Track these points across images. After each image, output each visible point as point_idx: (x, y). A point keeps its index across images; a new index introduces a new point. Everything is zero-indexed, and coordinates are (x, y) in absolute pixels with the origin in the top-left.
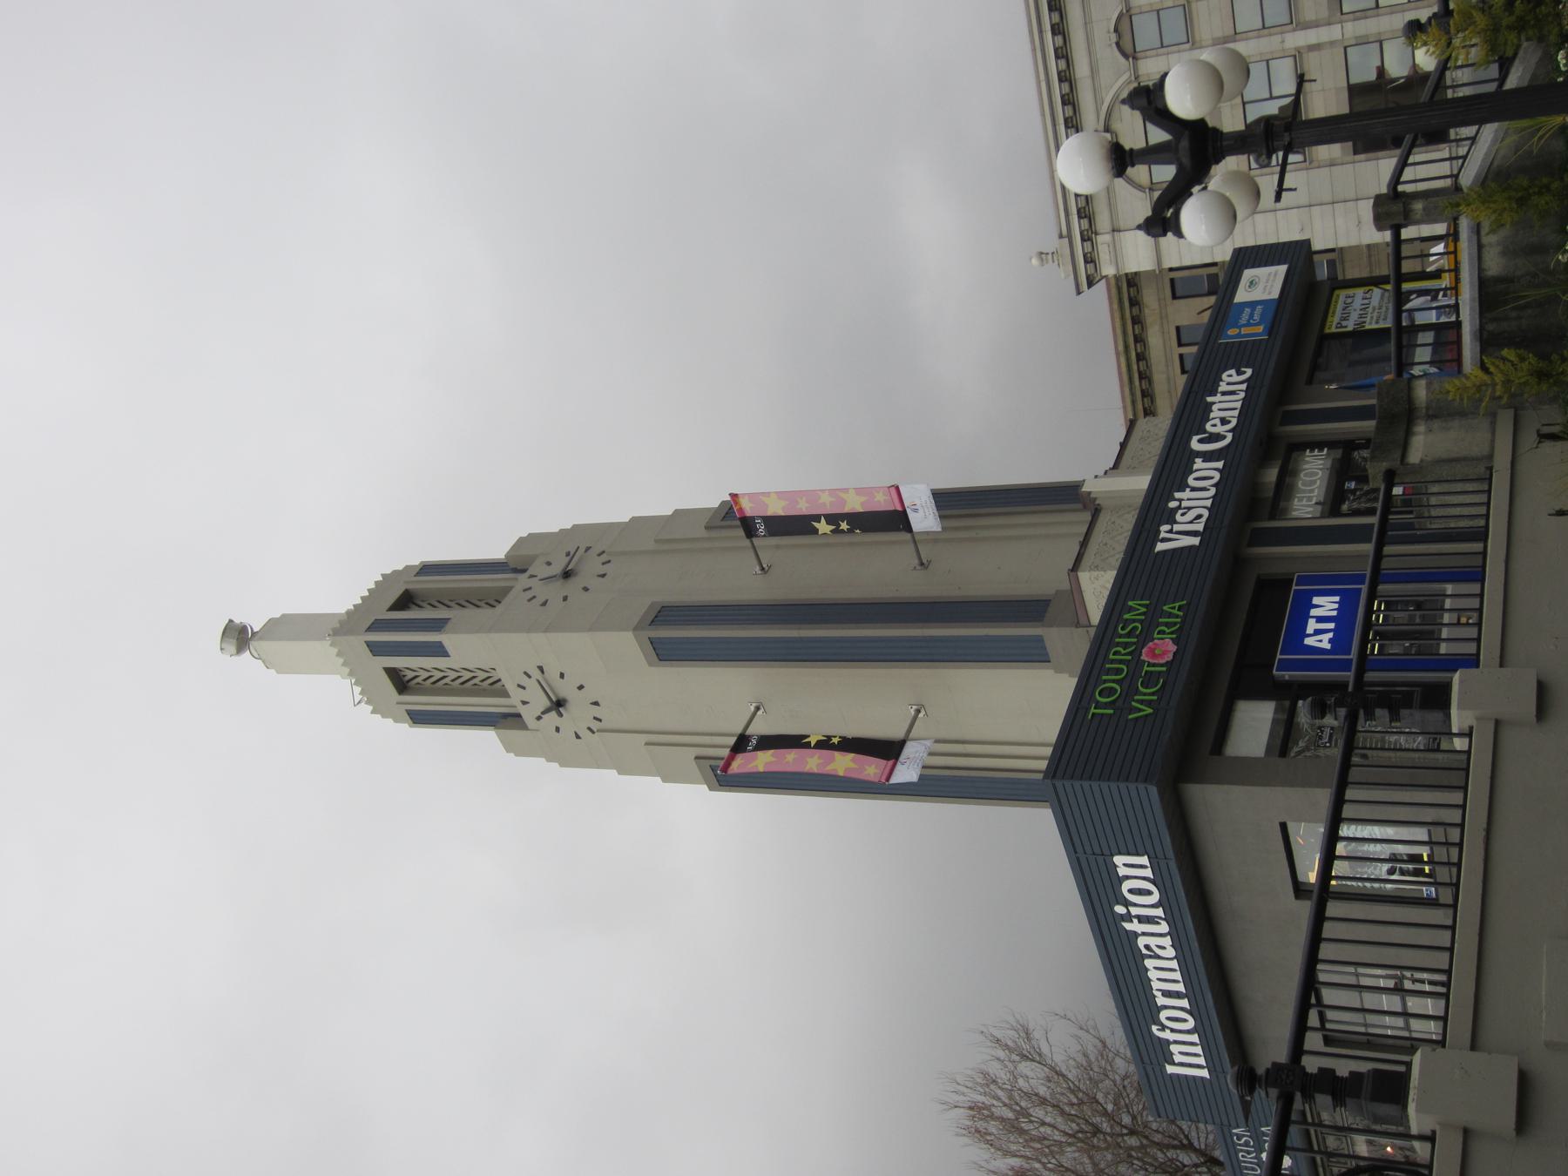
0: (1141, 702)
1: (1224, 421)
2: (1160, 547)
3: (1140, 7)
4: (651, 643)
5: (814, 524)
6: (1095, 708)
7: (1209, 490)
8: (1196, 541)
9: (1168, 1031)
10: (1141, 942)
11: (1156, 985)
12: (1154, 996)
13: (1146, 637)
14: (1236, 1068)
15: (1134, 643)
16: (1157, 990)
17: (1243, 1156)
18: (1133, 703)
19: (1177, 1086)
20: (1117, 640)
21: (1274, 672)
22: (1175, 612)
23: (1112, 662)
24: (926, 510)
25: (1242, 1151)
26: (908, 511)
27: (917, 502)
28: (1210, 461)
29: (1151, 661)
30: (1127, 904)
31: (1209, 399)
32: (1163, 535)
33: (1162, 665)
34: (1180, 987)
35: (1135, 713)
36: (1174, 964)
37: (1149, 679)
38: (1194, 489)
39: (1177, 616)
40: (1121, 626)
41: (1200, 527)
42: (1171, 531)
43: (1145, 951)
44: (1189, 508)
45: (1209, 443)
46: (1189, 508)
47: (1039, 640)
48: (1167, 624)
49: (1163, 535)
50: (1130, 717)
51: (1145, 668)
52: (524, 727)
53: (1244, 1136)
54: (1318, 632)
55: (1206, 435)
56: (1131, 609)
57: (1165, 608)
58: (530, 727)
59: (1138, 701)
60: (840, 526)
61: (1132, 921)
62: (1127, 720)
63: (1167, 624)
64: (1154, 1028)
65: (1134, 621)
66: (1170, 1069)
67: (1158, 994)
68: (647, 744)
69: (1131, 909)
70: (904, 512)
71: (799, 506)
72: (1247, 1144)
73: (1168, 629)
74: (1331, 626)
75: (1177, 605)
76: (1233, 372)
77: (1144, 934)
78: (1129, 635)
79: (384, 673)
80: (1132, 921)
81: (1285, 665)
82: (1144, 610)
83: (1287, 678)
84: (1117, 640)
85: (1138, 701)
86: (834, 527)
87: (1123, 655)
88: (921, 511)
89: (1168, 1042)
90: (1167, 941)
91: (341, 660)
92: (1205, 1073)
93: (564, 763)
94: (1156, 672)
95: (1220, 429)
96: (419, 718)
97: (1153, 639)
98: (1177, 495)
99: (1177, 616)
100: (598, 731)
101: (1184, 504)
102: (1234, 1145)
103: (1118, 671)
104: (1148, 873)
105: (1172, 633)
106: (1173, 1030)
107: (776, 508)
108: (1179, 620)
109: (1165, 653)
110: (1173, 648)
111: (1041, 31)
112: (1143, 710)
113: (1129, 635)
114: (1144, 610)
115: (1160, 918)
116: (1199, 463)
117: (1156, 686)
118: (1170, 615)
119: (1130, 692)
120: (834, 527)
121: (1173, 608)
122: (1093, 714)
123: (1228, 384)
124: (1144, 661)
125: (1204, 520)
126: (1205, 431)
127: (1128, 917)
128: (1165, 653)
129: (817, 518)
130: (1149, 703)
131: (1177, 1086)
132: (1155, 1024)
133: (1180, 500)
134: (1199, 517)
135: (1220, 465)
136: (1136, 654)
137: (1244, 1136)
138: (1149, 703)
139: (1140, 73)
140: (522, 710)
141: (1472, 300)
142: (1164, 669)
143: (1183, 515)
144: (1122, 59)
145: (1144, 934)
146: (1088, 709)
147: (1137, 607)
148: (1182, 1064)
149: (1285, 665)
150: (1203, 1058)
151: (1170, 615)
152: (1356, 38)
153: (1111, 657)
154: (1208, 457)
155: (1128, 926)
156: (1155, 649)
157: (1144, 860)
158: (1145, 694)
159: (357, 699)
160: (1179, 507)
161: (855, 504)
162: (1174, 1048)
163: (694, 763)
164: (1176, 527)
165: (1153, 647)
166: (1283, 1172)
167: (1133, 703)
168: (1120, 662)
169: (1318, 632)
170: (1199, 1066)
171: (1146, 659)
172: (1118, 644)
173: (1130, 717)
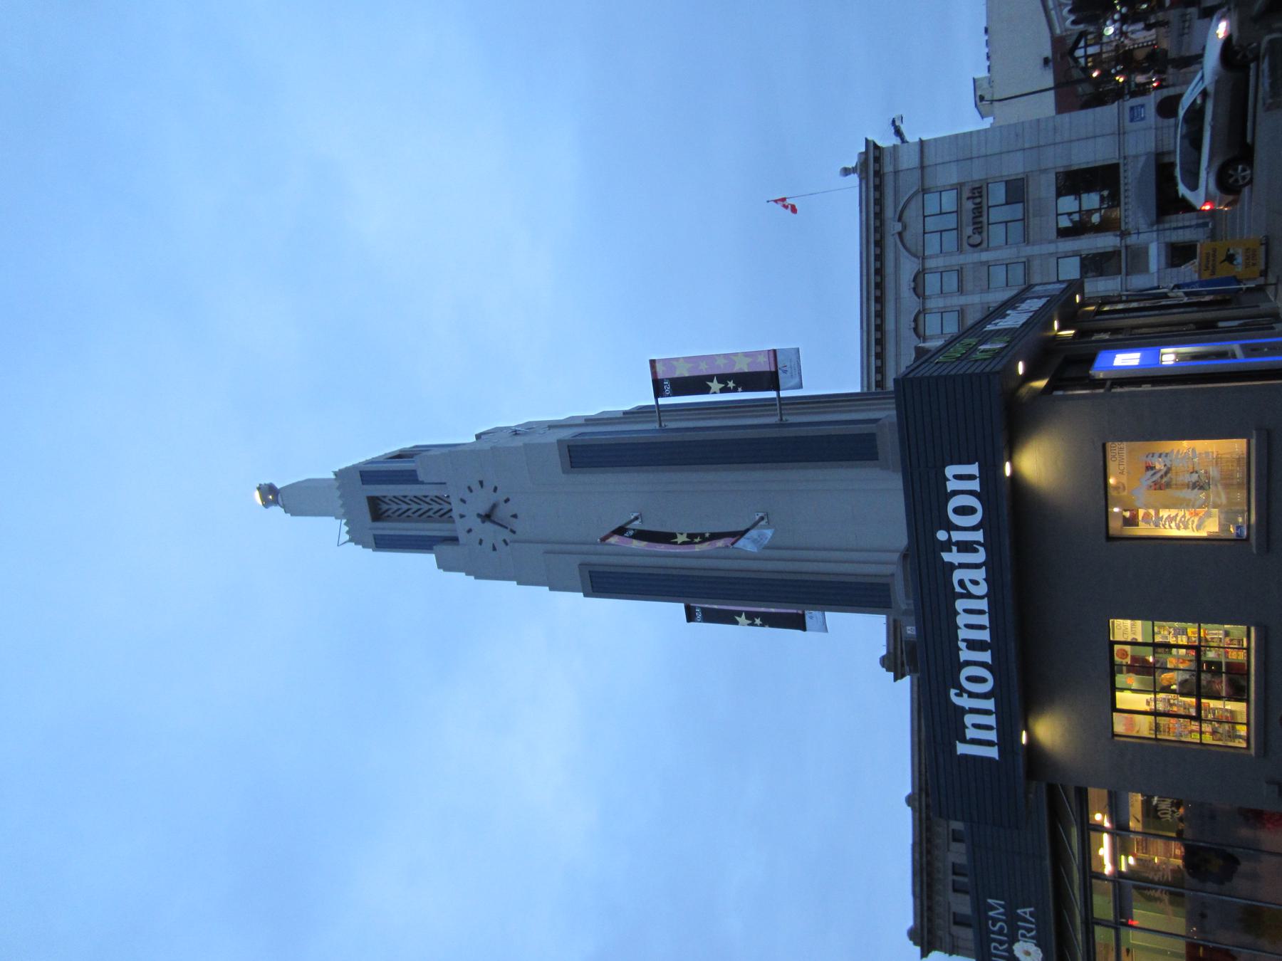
3: (931, 268)
5: (708, 383)
9: (965, 695)
11: (963, 634)
12: (959, 649)
14: (1180, 195)
16: (964, 640)
17: (996, 948)
22: (1028, 916)
24: (793, 371)
25: (995, 940)
26: (780, 372)
27: (788, 364)
43: (958, 589)
53: (1000, 920)
56: (992, 908)
60: (728, 384)
61: (950, 551)
63: (1024, 928)
66: (962, 749)
67: (962, 645)
70: (776, 373)
71: (700, 368)
72: (1000, 932)
75: (1028, 910)
77: (962, 566)
80: (950, 551)
82: (1002, 910)
86: (723, 385)
87: (1001, 951)
88: (788, 374)
90: (980, 574)
91: (341, 502)
92: (993, 753)
93: (479, 575)
96: (383, 543)
100: (511, 542)
102: (989, 932)
106: (972, 695)
107: (683, 372)
111: (868, 299)
114: (1002, 910)
115: (978, 543)
120: (723, 385)
127: (947, 546)
129: (710, 378)
132: (954, 688)
137: (1000, 920)
139: (926, 307)
144: (916, 298)
145: (962, 566)
150: (994, 732)
152: (1073, 251)
155: (946, 557)
157: (973, 469)
159: (342, 540)
161: (743, 366)
170: (989, 743)
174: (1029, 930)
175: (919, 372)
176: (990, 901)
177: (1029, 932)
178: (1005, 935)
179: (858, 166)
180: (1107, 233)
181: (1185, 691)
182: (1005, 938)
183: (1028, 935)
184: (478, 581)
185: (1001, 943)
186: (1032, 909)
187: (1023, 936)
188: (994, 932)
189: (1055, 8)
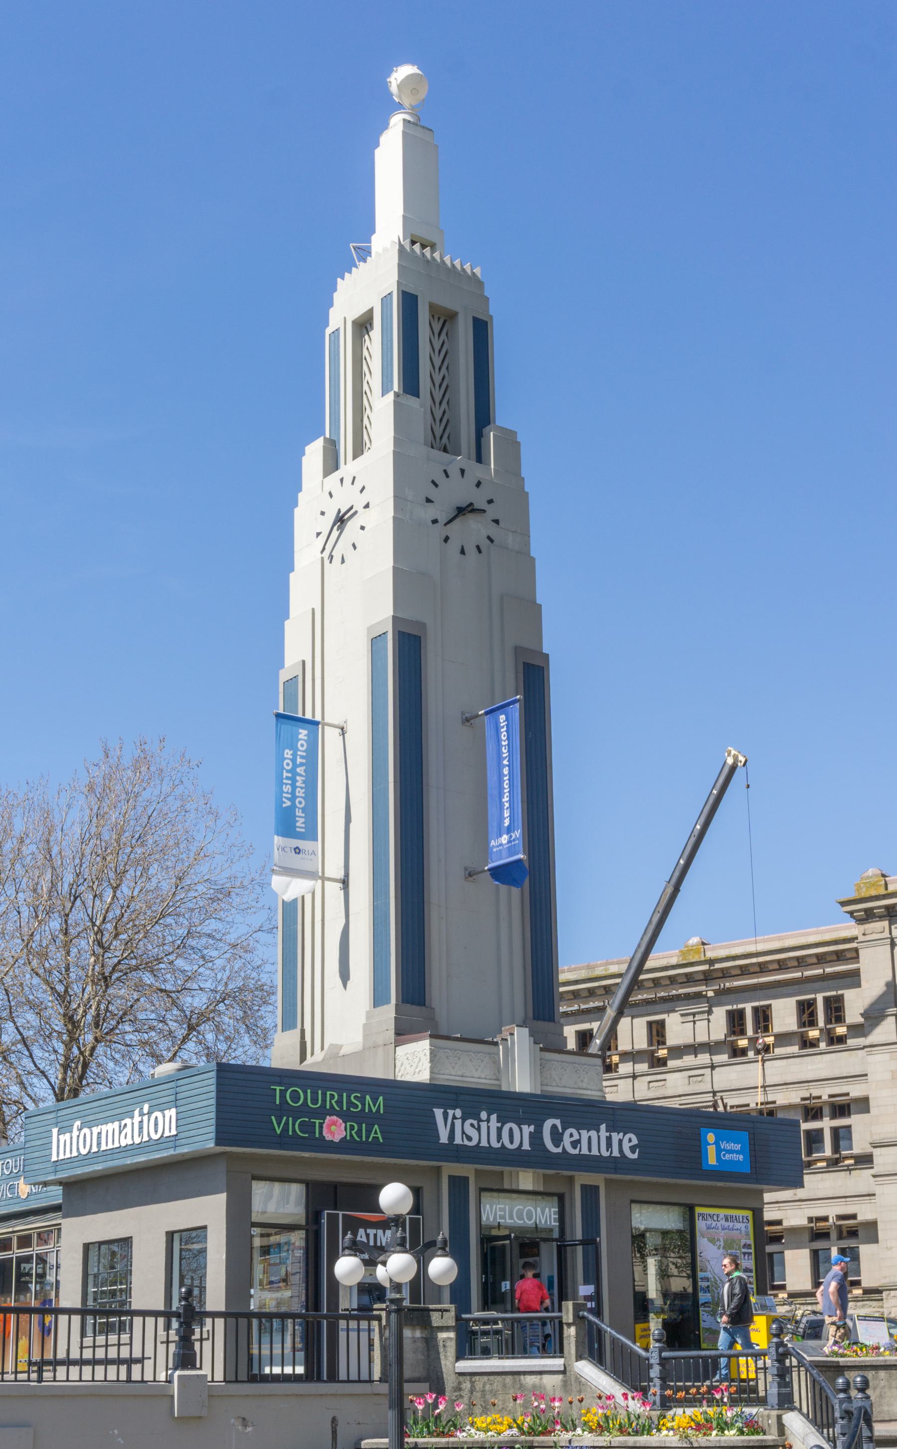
0: (287, 1123)
1: (575, 1144)
2: (438, 1113)
4: (384, 634)
6: (280, 1090)
7: (498, 1142)
8: (444, 1138)
10: (128, 1121)
13: (346, 1116)
15: (342, 1108)
17: (332, 1097)
18: (285, 1118)
19: (44, 1135)
20: (345, 1094)
21: (326, 1211)
22: (372, 1135)
23: (324, 1095)
28: (530, 1138)
29: (324, 1126)
30: (149, 1113)
31: (603, 1127)
32: (451, 1112)
33: (321, 1133)
34: (103, 1147)
35: (276, 1120)
36: (116, 1145)
37: (308, 1127)
38: (499, 1130)
39: (368, 1137)
40: (359, 1095)
41: (458, 1140)
42: (454, 1117)
44: (479, 1129)
45: (551, 1133)
46: (479, 1129)
47: (388, 1002)
48: (360, 1130)
49: (451, 1112)
50: (273, 1118)
51: (317, 1121)
52: (327, 473)
54: (368, 1235)
55: (561, 1131)
56: (375, 1100)
57: (376, 1127)
58: (325, 480)
59: (287, 1120)
62: (270, 1116)
63: (360, 1130)
64: (78, 1123)
65: (363, 1105)
68: (313, 610)
69: (147, 1116)
73: (356, 1133)
74: (616, 1153)
75: (379, 1135)
76: (635, 1141)
78: (350, 1103)
79: (370, 307)
81: (333, 1219)
82: (374, 1110)
83: (323, 1221)
84: (345, 1094)
85: (287, 1120)
87: (330, 1102)
89: (71, 1132)
92: (54, 1158)
94: (315, 1129)
95: (567, 1141)
97: (345, 1122)
98: (494, 1117)
99: (368, 1137)
101: (484, 1125)
103: (314, 1101)
104: (167, 1134)
105: (351, 1135)
108: (364, 1139)
109: (332, 1133)
110: (337, 1139)
112: (279, 1127)
113: (350, 1103)
114: (374, 1110)
115: (611, 1153)
116: (527, 1129)
117: (301, 1132)
118: (369, 1132)
119: (296, 1113)
121: (376, 1133)
122: (275, 1089)
123: (620, 1141)
124: (324, 1119)
125: (466, 1142)
126: (564, 1129)
128: (332, 1133)
130: (285, 1129)
131: (44, 1135)
133: (488, 1121)
134: (470, 1139)
135: (526, 1146)
136: (332, 1111)
138: (285, 1129)
140: (336, 475)
141: (504, 1367)
142: (317, 1135)
143: (472, 1125)
146: (280, 1084)
147: (376, 1105)
148: (58, 1141)
149: (333, 1219)
151: (369, 1132)
153: (328, 1093)
154: (536, 1138)
156: (336, 1125)
158: (294, 1125)
160: (480, 1120)
162: (68, 1135)
163: (298, 660)
164: (458, 1123)
165: (338, 1123)
166: (298, 829)
167: (285, 1118)
168: (324, 1101)
169: (368, 1235)
171: (326, 1121)
172: (341, 1096)
173: (273, 1118)
174: (359, 1133)
175: (821, 1400)
176: (381, 1098)
177: (356, 1133)
178: (348, 1109)
179: (588, 1040)
180: (528, 1170)
181: (426, 1313)
182: (345, 1108)
183: (353, 1132)
184: (303, 488)
185: (340, 1102)
186: (381, 1140)
187: (352, 1128)
188: (349, 1097)
189: (685, 1386)
